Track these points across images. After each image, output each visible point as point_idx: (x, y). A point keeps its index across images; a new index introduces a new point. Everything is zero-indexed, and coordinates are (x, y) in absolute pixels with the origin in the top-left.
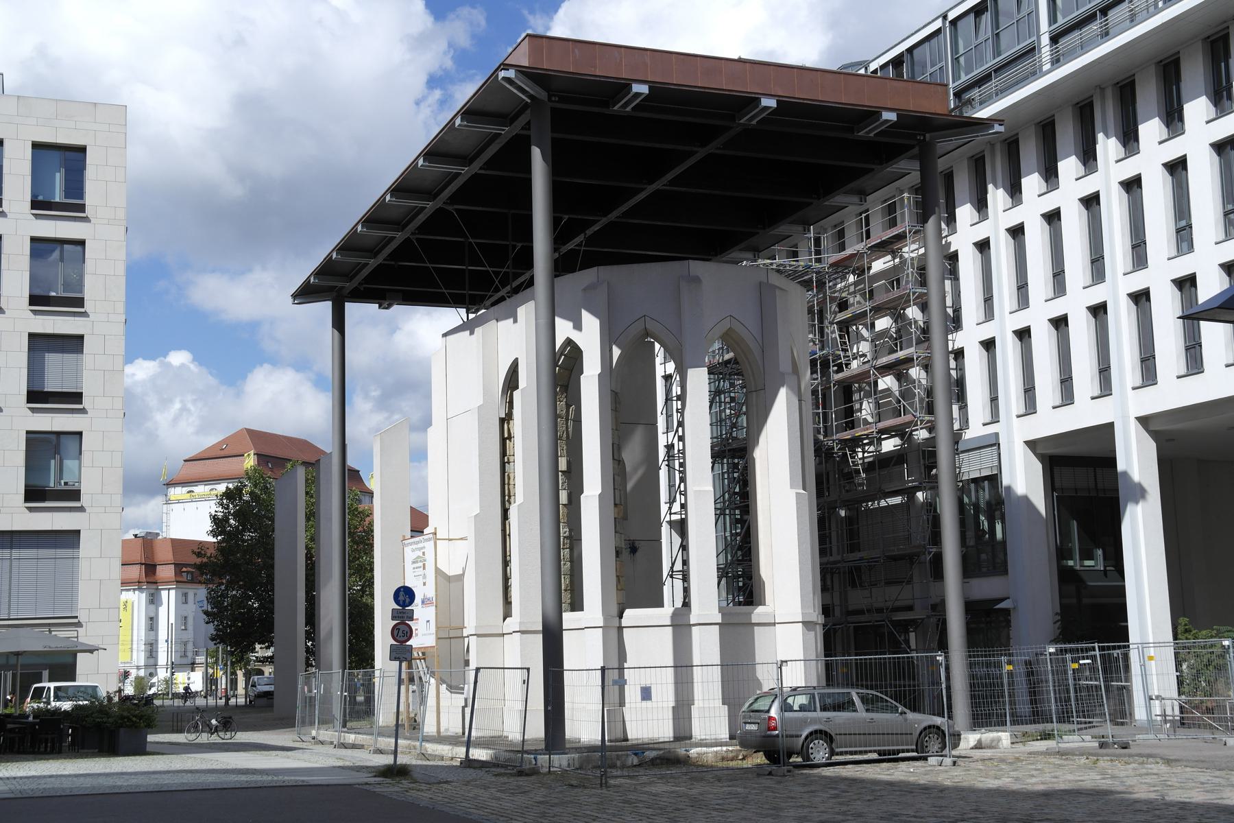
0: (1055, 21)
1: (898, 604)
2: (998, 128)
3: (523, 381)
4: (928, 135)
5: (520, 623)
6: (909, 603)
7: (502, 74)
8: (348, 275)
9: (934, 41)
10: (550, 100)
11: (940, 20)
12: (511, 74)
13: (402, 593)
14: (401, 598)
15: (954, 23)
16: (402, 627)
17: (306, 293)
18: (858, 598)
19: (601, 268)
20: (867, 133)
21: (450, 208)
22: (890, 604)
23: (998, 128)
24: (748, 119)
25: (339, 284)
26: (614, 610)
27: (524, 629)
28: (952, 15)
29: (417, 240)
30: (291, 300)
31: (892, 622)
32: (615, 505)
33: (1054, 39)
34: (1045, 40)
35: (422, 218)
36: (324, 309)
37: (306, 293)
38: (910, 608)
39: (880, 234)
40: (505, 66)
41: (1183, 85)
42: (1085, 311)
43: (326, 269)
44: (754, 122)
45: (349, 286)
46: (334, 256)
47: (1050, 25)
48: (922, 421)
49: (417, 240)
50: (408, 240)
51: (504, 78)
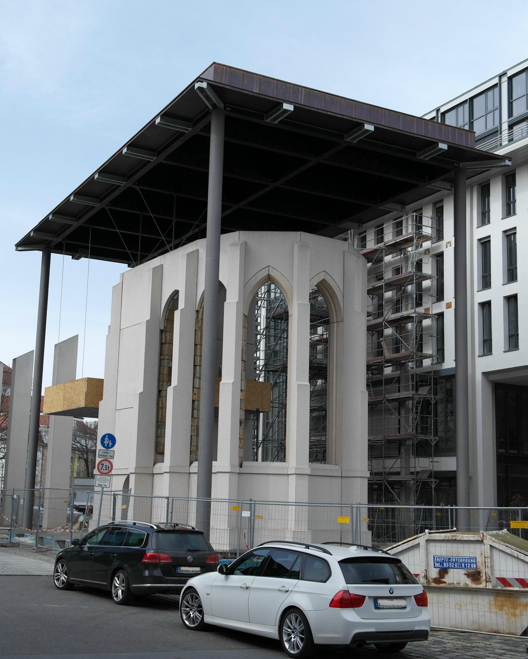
0: (512, 116)
1: (392, 470)
2: (508, 163)
3: (181, 305)
4: (460, 163)
5: (170, 467)
6: (398, 470)
7: (197, 85)
8: (56, 233)
9: (490, 93)
10: (225, 109)
11: (435, 112)
12: (204, 85)
13: (107, 439)
14: (106, 442)
15: (443, 114)
16: (106, 463)
17: (26, 244)
18: (392, 464)
19: (242, 232)
20: (424, 157)
21: (137, 188)
22: (387, 470)
23: (508, 163)
24: (351, 139)
25: (49, 239)
26: (237, 462)
27: (172, 471)
28: (442, 110)
29: (110, 210)
30: (15, 248)
31: (387, 481)
32: (241, 390)
33: (511, 127)
34: (505, 126)
35: (116, 193)
36: (37, 255)
37: (26, 244)
38: (398, 474)
39: (389, 237)
40: (199, 79)
41: (517, 188)
42: (502, 298)
43: (43, 227)
44: (355, 142)
45: (56, 240)
46: (32, 234)
47: (509, 117)
48: (417, 356)
49: (110, 210)
50: (103, 210)
51: (199, 88)
